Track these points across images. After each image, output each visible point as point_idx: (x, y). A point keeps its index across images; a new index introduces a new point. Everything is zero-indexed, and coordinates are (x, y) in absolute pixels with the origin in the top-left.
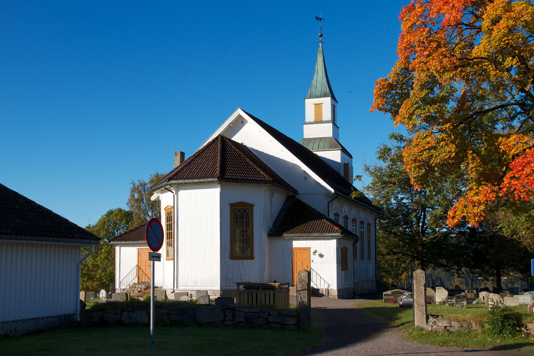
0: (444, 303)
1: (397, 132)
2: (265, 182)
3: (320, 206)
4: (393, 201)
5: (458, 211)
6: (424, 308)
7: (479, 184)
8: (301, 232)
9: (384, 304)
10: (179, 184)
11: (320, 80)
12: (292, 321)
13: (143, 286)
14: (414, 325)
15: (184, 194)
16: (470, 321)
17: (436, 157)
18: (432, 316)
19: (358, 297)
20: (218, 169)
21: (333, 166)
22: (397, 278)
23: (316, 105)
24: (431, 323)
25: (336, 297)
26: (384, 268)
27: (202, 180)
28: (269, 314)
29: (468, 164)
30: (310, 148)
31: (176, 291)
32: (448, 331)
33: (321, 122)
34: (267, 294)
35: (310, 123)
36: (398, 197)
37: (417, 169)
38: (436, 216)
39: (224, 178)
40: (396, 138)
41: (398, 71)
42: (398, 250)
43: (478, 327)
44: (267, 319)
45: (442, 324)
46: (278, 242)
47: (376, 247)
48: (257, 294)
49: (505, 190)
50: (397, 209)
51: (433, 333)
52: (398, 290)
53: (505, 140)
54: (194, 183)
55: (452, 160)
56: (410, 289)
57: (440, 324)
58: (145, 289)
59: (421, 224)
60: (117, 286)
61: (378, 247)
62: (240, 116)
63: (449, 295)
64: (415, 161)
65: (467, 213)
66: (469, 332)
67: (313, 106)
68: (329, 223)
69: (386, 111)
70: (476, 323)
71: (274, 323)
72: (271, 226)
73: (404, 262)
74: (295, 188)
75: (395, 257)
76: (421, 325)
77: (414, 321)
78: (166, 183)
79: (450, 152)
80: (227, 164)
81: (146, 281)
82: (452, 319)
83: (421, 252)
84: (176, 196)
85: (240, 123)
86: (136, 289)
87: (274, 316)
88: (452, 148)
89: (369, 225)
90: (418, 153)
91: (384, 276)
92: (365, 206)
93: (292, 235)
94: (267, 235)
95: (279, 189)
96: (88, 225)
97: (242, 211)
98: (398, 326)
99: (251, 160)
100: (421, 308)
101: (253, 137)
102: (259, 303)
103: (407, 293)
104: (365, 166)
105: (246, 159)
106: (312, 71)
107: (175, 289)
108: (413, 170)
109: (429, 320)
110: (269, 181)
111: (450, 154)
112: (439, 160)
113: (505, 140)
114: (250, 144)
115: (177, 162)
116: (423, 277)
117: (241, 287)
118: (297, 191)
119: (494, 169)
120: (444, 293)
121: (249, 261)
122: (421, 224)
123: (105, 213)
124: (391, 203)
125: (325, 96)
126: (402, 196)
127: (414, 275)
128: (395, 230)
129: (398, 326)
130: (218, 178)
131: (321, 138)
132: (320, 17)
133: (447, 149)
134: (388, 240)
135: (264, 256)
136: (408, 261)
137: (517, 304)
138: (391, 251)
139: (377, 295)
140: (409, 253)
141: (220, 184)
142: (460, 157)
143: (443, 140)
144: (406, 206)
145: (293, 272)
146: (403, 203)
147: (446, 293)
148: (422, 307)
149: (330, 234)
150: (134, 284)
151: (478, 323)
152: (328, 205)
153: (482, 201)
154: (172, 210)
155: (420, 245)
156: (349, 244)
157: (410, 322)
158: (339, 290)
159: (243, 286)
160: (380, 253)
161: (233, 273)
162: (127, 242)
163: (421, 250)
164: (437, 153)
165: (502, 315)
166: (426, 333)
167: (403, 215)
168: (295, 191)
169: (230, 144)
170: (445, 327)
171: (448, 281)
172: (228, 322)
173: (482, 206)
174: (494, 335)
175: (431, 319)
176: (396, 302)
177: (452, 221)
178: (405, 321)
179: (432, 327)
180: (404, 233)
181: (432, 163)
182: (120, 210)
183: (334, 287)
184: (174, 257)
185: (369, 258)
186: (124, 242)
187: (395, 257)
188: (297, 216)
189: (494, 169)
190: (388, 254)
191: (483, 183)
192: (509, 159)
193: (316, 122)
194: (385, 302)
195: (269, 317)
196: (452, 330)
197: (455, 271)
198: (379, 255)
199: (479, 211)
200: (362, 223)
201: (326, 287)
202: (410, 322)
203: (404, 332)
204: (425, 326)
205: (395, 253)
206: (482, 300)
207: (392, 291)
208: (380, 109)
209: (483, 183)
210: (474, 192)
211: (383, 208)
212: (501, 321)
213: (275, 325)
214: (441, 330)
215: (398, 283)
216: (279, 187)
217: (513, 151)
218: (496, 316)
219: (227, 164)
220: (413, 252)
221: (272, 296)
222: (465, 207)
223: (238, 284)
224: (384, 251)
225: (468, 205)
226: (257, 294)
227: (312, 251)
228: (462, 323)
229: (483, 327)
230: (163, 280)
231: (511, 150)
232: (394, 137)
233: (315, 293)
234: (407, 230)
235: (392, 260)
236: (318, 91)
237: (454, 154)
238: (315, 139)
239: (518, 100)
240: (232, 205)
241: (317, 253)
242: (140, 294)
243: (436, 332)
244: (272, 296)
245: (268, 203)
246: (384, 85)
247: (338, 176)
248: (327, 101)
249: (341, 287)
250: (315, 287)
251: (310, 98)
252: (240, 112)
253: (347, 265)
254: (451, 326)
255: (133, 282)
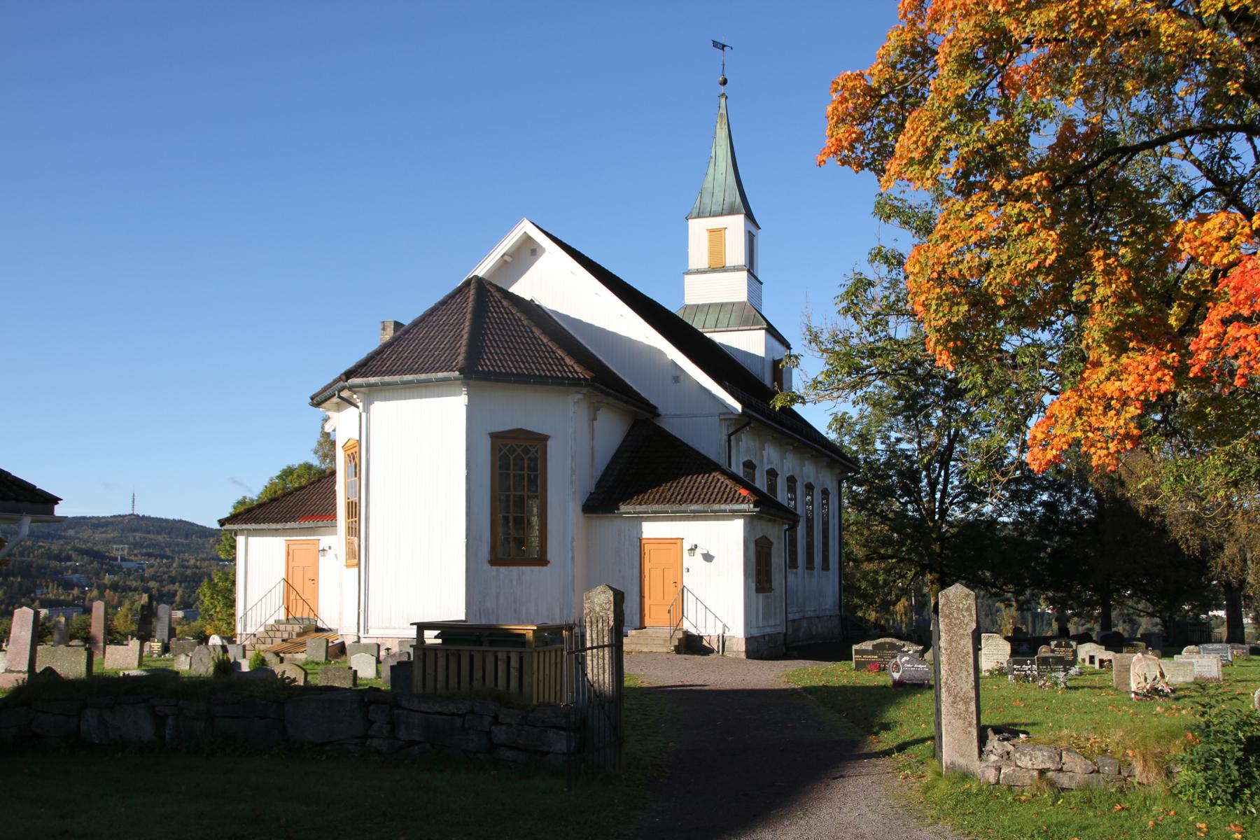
0: (1001, 672)
1: (888, 246)
2: (576, 383)
3: (708, 441)
4: (879, 445)
5: (1044, 438)
6: (973, 707)
7: (1120, 348)
8: (662, 500)
9: (854, 674)
10: (369, 386)
11: (720, 178)
12: (559, 743)
13: (297, 628)
14: (936, 753)
15: (383, 410)
16: (1125, 755)
17: (1000, 266)
18: (997, 730)
19: (795, 654)
20: (463, 350)
21: (746, 364)
22: (887, 611)
23: (711, 231)
24: (993, 758)
25: (743, 656)
26: (859, 588)
27: (423, 376)
28: (495, 720)
29: (1094, 285)
30: (697, 325)
31: (363, 641)
32: (1052, 784)
33: (724, 269)
34: (502, 656)
35: (698, 272)
36: (889, 438)
37: (946, 303)
38: (988, 452)
39: (477, 373)
40: (886, 260)
41: (894, 56)
42: (890, 551)
43: (1152, 776)
44: (489, 733)
45: (1031, 760)
46: (607, 527)
47: (842, 544)
48: (472, 658)
49: (1203, 356)
50: (888, 464)
51: (999, 795)
52: (888, 640)
53: (1195, 228)
54: (405, 383)
55: (1047, 274)
56: (923, 637)
57: (1025, 762)
58: (299, 635)
59: (938, 495)
60: (239, 629)
61: (847, 544)
62: (527, 239)
63: (1014, 653)
64: (940, 281)
65: (1085, 432)
66: (1121, 790)
67: (706, 235)
68: (727, 482)
69: (861, 166)
70: (1145, 761)
71: (509, 747)
72: (590, 486)
73: (902, 576)
74: (652, 401)
75: (883, 565)
76: (962, 761)
77: (936, 738)
78: (341, 383)
79: (1040, 251)
80: (487, 339)
81: (305, 616)
82: (1064, 744)
83: (940, 555)
84: (364, 415)
85: (526, 253)
86: (278, 634)
87: (509, 725)
88: (1049, 240)
89: (825, 493)
90: (950, 256)
91: (860, 607)
92: (816, 450)
93: (639, 508)
94: (579, 509)
95: (611, 400)
96: (240, 498)
97: (519, 451)
98: (887, 753)
99: (544, 333)
100: (961, 706)
101: (559, 287)
102: (477, 684)
103: (911, 648)
104: (809, 329)
105: (534, 329)
106: (709, 159)
107: (361, 634)
108: (934, 307)
109: (989, 747)
110: (585, 379)
111: (1042, 256)
112: (1008, 276)
113: (1195, 228)
114: (549, 302)
115: (389, 335)
116: (968, 609)
117: (431, 637)
118: (656, 408)
119: (1162, 309)
120: (1000, 647)
121: (536, 569)
122: (938, 495)
123: (278, 473)
124: (876, 450)
125: (732, 211)
126: (899, 435)
127: (941, 602)
128: (882, 505)
129: (887, 753)
130: (461, 371)
131: (722, 305)
132: (722, 41)
133: (1033, 242)
134: (869, 529)
135: (573, 558)
136: (910, 575)
137: (1190, 679)
138: (875, 552)
139: (838, 652)
140: (913, 556)
141: (467, 385)
142: (1070, 265)
143: (1021, 219)
144: (907, 457)
145: (642, 597)
146: (901, 450)
147: (1007, 647)
148: (967, 703)
149: (728, 507)
150: (278, 622)
151: (1152, 764)
152: (729, 441)
153: (1132, 395)
154: (357, 449)
155: (936, 540)
156: (775, 533)
157: (923, 740)
158: (748, 640)
159: (436, 632)
160: (849, 557)
161: (498, 596)
162: (262, 526)
163: (938, 550)
164: (1004, 257)
165: (1239, 741)
166: (980, 790)
167: (900, 474)
168: (652, 410)
169: (498, 295)
170: (1042, 772)
171: (987, 616)
172: (375, 743)
173: (1132, 409)
174: (1213, 804)
175: (993, 742)
176: (884, 669)
177: (1040, 456)
178: (906, 737)
179: (999, 769)
180: (902, 514)
181: (990, 284)
182: (308, 467)
183: (737, 631)
184: (356, 556)
185: (826, 566)
186: (254, 526)
187: (883, 565)
188: (652, 465)
189: (1162, 309)
190: (869, 559)
191: (1131, 345)
192: (1203, 283)
193: (712, 270)
194: (857, 669)
195: (495, 729)
196: (1064, 780)
197: (1010, 595)
198: (849, 560)
199: (1122, 422)
200: (809, 487)
201: (720, 632)
202: (923, 740)
203: (906, 777)
204: (976, 766)
205: (883, 558)
206: (1087, 663)
207: (875, 642)
208: (845, 162)
209: (1131, 345)
210: (1106, 370)
211: (857, 459)
212: (1238, 762)
213: (509, 754)
214: (1028, 781)
215: (887, 620)
216: (608, 395)
217: (1216, 258)
218: (1217, 741)
219: (487, 339)
220: (922, 556)
221: (514, 662)
222: (1080, 412)
223: (422, 627)
224: (860, 552)
225: (1078, 415)
226: (472, 658)
227: (687, 546)
228: (1098, 759)
229: (1169, 774)
230: (340, 613)
231: (1212, 255)
232: (880, 256)
233: (691, 645)
234: (909, 506)
235: (876, 572)
236: (717, 202)
237: (1052, 257)
238: (710, 305)
239: (1202, 158)
240: (496, 437)
241: (698, 552)
242: (286, 645)
243: (1010, 787)
244: (514, 662)
245: (587, 433)
246: (854, 87)
247: (757, 387)
248: (737, 223)
249: (756, 632)
250: (693, 631)
251: (699, 216)
252: (527, 227)
253: (769, 581)
254: (1060, 770)
255: (276, 617)
